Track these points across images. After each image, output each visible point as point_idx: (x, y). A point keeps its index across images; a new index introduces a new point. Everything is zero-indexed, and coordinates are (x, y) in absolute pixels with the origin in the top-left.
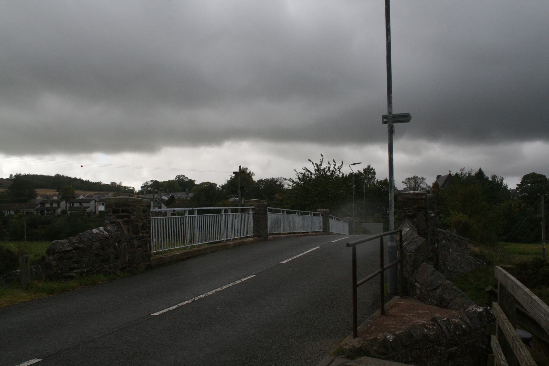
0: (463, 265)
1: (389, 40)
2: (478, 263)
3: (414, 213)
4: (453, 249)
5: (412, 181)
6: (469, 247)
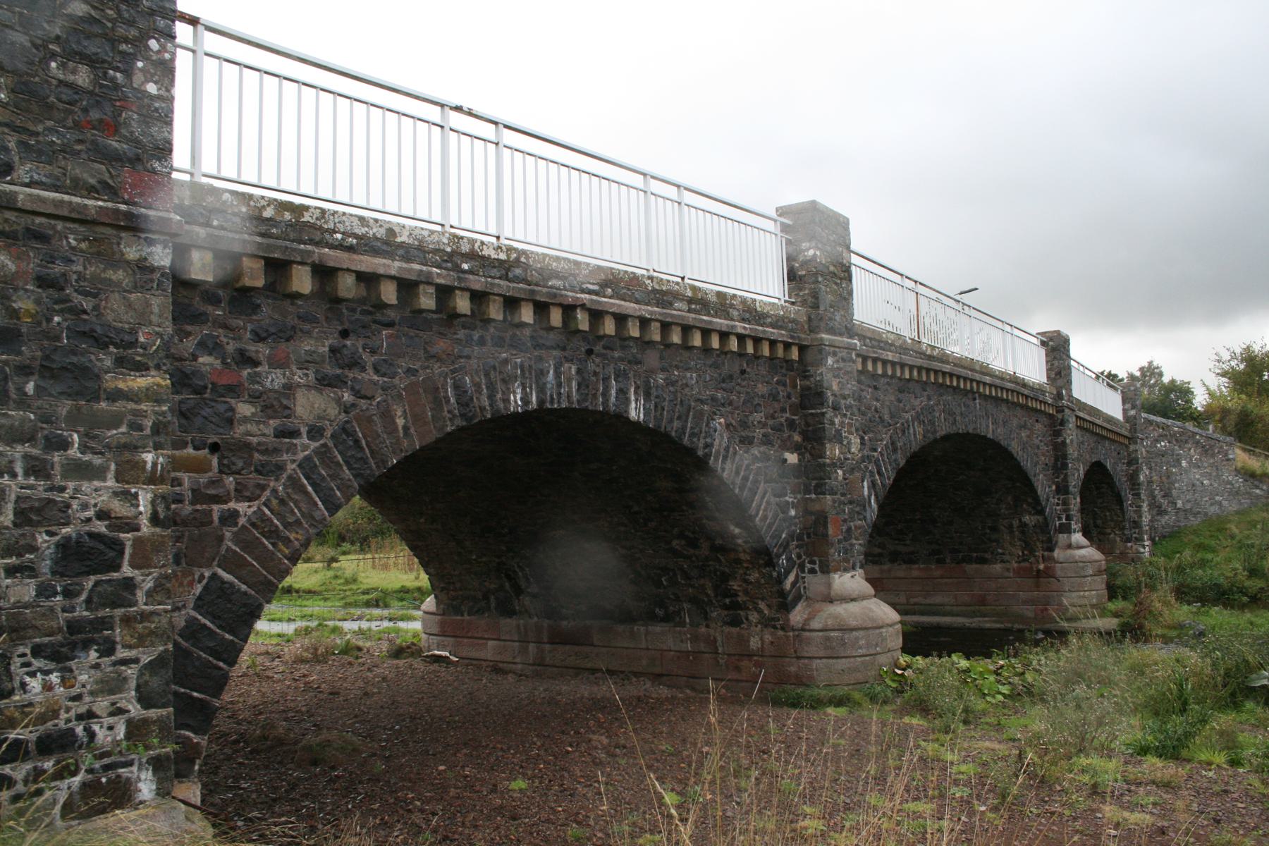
0: (1217, 498)
1: (184, 18)
2: (1258, 491)
4: (1191, 459)
6: (1231, 457)
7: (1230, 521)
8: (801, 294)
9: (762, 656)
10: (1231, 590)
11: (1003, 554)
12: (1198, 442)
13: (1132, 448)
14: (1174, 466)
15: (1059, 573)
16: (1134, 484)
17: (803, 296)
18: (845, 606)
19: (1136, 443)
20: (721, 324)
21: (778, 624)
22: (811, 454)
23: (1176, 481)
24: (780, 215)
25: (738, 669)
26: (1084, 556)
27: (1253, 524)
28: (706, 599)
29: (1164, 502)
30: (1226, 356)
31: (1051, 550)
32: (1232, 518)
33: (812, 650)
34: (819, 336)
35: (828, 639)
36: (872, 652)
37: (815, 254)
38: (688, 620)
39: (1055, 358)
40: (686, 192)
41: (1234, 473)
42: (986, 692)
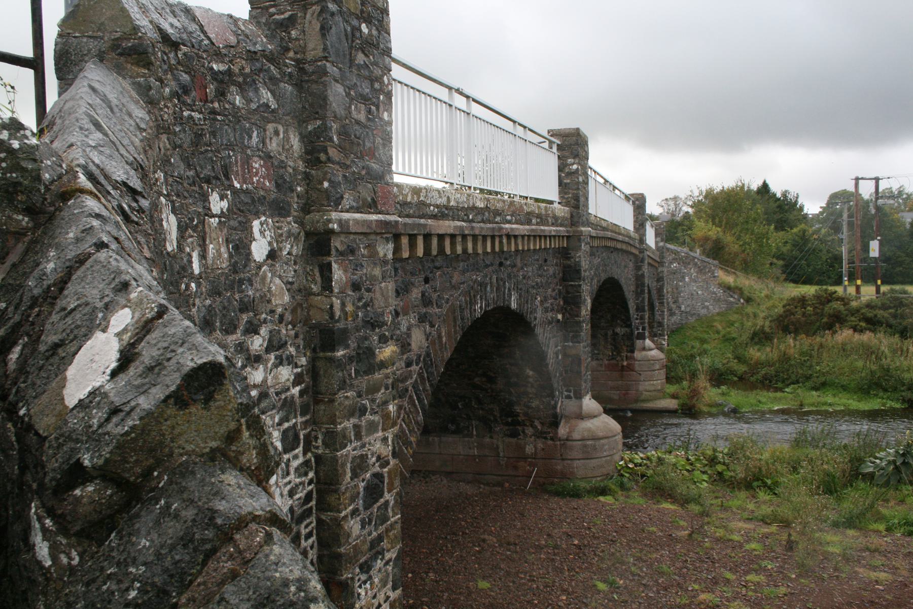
0: (707, 304)
2: (731, 299)
3: (290, 13)
5: (671, 203)
7: (715, 321)
8: (566, 196)
9: (534, 458)
10: (726, 372)
11: (599, 354)
12: (696, 264)
13: (660, 269)
14: (681, 281)
15: (637, 368)
16: (660, 296)
17: (567, 198)
18: (591, 421)
19: (663, 266)
20: (550, 231)
21: (548, 436)
22: (569, 314)
23: (682, 291)
24: (551, 136)
25: (516, 468)
26: (654, 356)
27: (732, 324)
28: (492, 418)
29: (674, 306)
30: (696, 193)
31: (633, 352)
32: (716, 318)
33: (575, 454)
34: (579, 229)
35: (585, 446)
36: (612, 453)
37: (578, 168)
38: (475, 433)
39: (639, 213)
40: (473, 104)
41: (717, 286)
42: (696, 480)
